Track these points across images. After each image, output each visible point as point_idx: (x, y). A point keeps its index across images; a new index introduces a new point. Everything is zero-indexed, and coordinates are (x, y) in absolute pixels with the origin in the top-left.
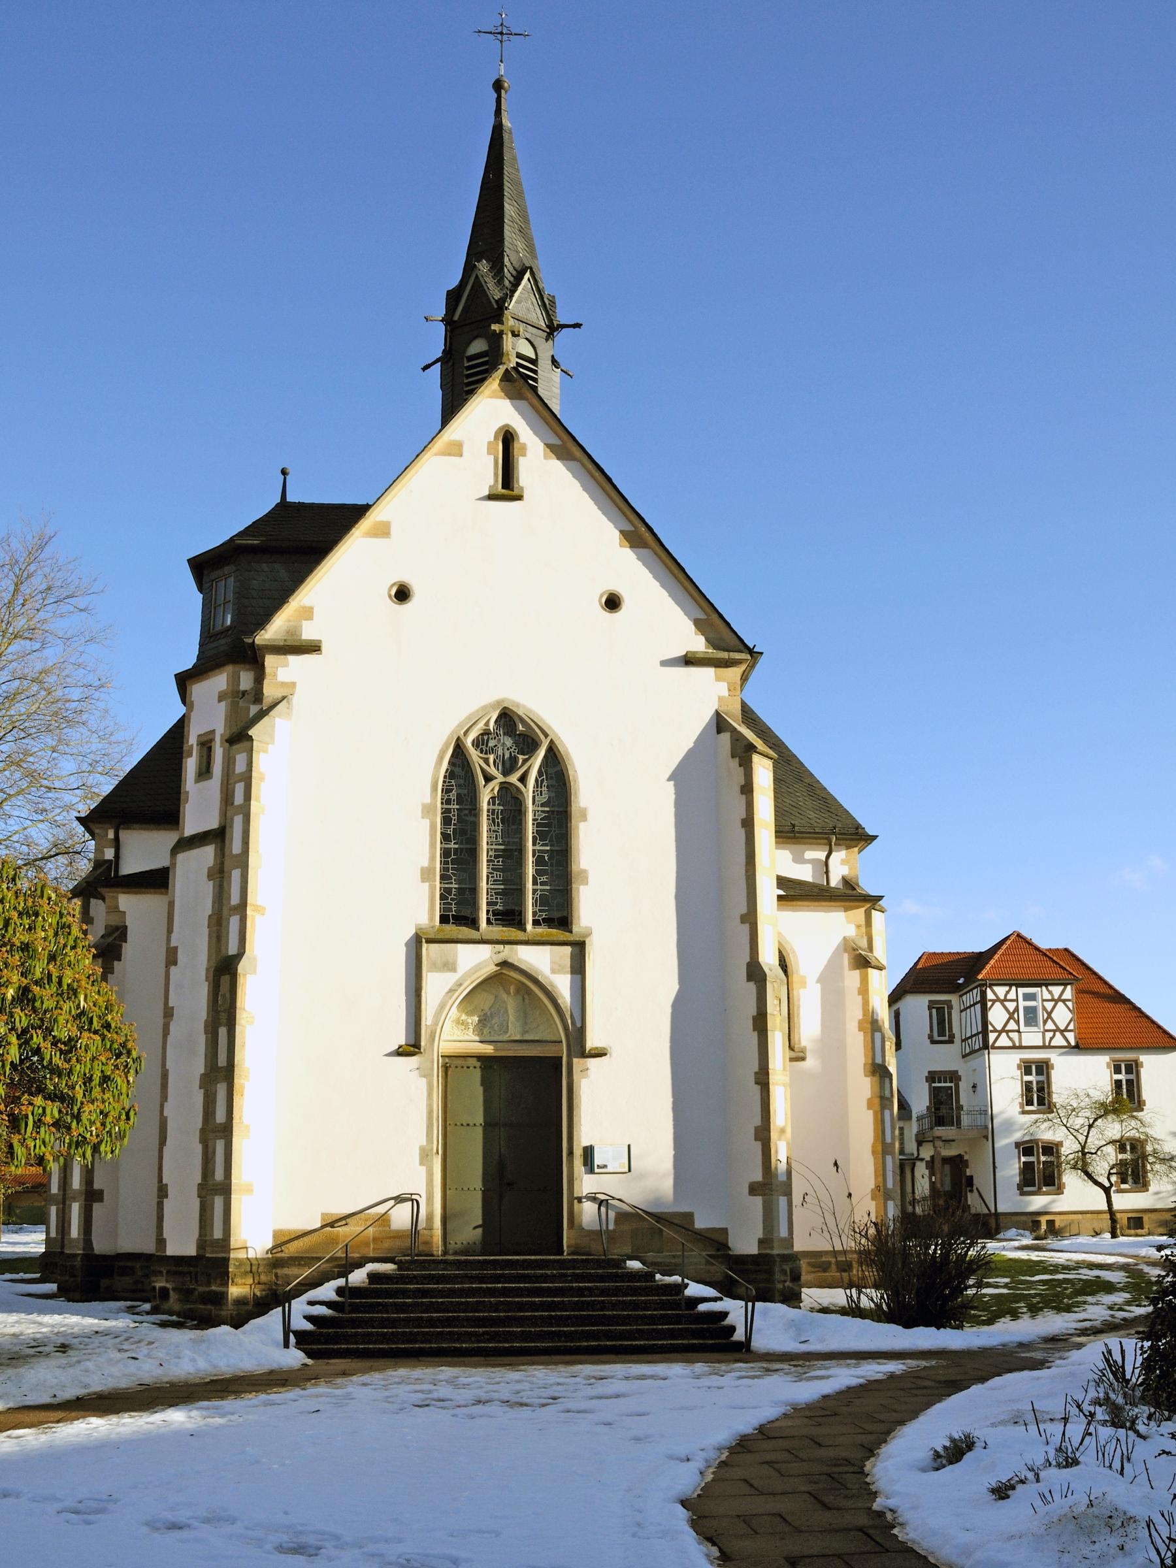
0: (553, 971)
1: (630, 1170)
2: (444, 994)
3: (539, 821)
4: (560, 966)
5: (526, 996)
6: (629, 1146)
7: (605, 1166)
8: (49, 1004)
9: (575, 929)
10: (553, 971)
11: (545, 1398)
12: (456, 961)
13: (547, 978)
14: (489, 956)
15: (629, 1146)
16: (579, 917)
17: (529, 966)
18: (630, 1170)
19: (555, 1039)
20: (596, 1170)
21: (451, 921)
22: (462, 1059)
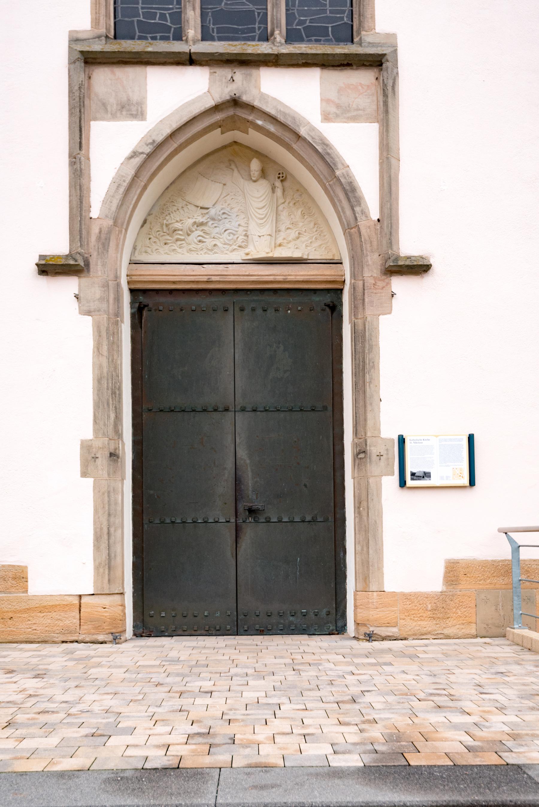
0: (326, 118)
1: (472, 482)
2: (122, 160)
3: (308, 24)
4: (338, 106)
5: (278, 184)
6: (471, 439)
7: (426, 475)
8: (164, 780)
9: (367, 37)
10: (326, 118)
11: (133, 717)
12: (145, 98)
13: (313, 129)
14: (206, 90)
15: (471, 439)
16: (373, 17)
17: (280, 107)
18: (472, 482)
19: (328, 256)
20: (410, 482)
21: (138, 34)
22: (240, 541)
